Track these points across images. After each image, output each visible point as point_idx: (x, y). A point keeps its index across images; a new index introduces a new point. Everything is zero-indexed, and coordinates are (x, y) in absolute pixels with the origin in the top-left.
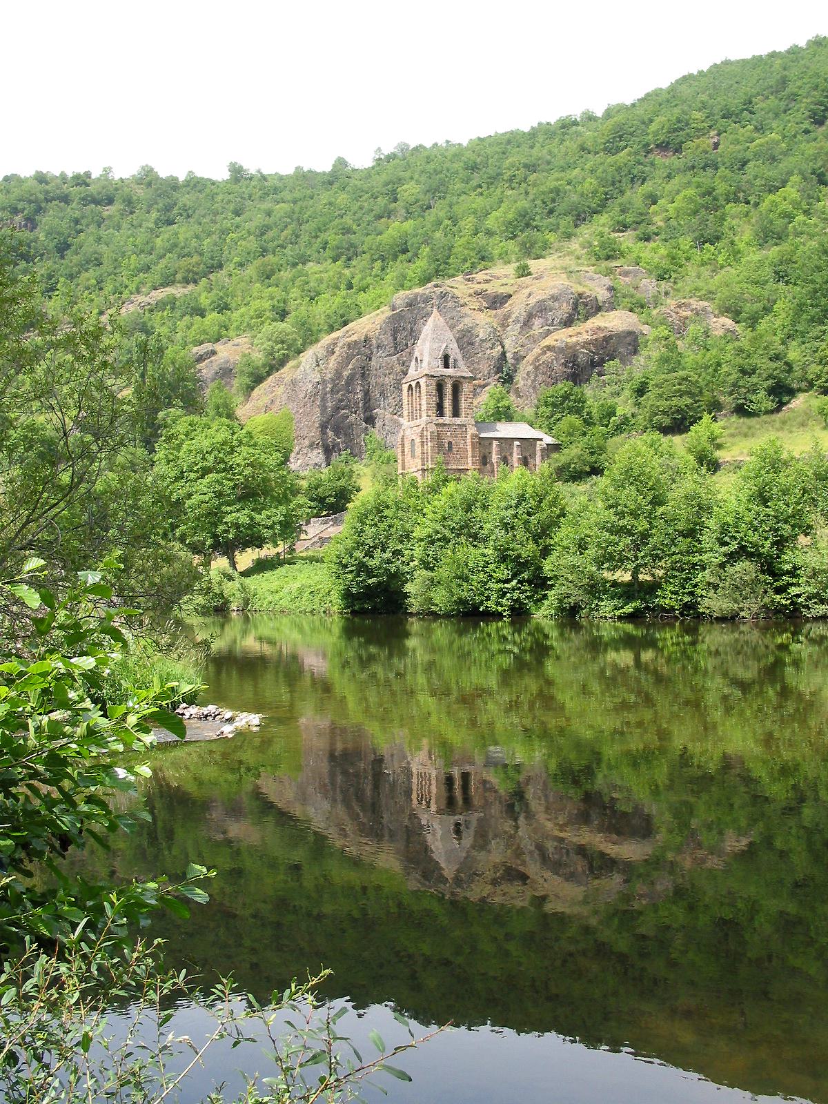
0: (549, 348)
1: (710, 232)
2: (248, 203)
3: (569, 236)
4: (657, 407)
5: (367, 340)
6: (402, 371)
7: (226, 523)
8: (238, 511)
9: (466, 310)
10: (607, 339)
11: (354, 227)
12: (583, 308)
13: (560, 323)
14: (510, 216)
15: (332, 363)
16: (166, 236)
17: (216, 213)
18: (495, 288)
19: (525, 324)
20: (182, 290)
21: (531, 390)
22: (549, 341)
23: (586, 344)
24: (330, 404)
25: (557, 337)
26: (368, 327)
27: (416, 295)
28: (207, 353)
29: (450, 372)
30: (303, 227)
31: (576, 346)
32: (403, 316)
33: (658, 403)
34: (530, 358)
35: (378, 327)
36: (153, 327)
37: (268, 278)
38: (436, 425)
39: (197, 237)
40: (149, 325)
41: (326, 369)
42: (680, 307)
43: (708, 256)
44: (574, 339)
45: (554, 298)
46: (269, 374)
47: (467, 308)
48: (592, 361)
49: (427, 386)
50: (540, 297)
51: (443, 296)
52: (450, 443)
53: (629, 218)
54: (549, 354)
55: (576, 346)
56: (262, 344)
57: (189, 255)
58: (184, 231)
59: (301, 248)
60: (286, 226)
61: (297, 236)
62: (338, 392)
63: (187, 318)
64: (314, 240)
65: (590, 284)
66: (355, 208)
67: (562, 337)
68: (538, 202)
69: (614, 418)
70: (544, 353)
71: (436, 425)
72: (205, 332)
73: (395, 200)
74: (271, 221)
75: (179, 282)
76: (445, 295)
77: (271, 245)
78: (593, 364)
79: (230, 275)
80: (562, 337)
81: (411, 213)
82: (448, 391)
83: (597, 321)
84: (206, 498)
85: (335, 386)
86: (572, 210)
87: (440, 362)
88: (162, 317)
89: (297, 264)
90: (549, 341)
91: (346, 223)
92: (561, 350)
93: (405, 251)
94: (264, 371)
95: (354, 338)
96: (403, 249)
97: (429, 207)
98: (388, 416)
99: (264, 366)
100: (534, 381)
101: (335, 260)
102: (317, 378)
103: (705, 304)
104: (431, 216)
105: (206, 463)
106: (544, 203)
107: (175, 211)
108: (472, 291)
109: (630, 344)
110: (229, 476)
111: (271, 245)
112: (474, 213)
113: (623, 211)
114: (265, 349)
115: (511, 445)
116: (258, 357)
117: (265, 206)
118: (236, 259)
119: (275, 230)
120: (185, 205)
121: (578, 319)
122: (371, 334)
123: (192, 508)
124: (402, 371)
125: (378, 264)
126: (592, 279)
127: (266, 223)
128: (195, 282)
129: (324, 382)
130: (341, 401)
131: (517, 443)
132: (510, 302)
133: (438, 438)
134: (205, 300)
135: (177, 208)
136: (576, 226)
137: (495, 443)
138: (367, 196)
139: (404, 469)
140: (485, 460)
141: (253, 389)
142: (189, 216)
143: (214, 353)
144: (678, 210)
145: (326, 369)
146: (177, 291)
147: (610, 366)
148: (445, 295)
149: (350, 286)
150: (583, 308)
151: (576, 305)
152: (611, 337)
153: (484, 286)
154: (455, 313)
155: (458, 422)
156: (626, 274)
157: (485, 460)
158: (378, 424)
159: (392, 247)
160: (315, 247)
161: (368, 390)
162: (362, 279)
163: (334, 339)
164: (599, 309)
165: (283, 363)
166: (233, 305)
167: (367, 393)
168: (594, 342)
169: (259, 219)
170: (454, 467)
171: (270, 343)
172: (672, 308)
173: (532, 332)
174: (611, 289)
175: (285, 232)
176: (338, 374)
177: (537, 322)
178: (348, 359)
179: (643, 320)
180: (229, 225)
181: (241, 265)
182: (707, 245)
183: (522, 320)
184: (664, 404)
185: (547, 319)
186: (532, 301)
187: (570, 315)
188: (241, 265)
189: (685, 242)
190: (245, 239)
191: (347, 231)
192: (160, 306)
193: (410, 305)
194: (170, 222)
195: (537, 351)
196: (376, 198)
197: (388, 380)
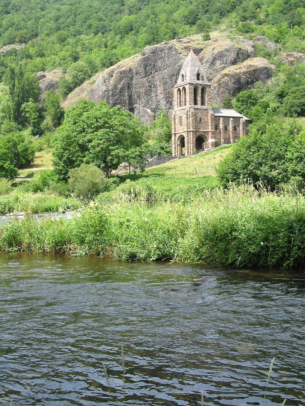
0: (226, 75)
1: (296, 20)
2: (47, 4)
3: (218, 23)
4: (294, 103)
5: (130, 70)
6: (149, 86)
7: (112, 155)
8: (117, 149)
9: (181, 56)
10: (255, 71)
11: (104, 18)
12: (241, 56)
13: (230, 63)
14: (186, 13)
15: (112, 81)
16: (8, 19)
17: (32, 9)
18: (194, 45)
19: (211, 63)
20: (19, 46)
21: (216, 96)
22: (225, 71)
23: (244, 73)
24: (111, 102)
25: (230, 70)
26: (131, 63)
27: (157, 48)
28: (41, 76)
29: (200, 82)
30: (77, 17)
31: (239, 74)
32: (150, 58)
33: (294, 101)
34: (215, 79)
35: (136, 63)
36: (7, 64)
37: (63, 41)
38: (194, 109)
39: (24, 20)
40: (5, 62)
41: (109, 84)
42: (288, 56)
43: (297, 31)
44: (238, 71)
45: (227, 50)
46: (75, 87)
47: (182, 55)
48: (248, 81)
49: (190, 89)
50: (220, 50)
51: (170, 48)
52: (200, 118)
53: (247, 15)
54: (226, 78)
55: (239, 74)
56: (71, 72)
57: (20, 29)
58: (16, 17)
59: (77, 28)
60: (69, 17)
61: (75, 22)
62: (115, 96)
63: (24, 60)
64: (84, 24)
65: (244, 44)
66: (103, 9)
67: (232, 70)
68: (200, 6)
69: (268, 109)
70: (223, 77)
71: (194, 109)
72: (36, 67)
73: (123, 5)
74: (60, 13)
75: (17, 42)
76: (171, 48)
77: (62, 26)
78: (248, 83)
79: (43, 40)
80: (232, 70)
81: (131, 12)
82: (199, 92)
83: (248, 62)
84: (101, 142)
85: (114, 92)
86: (218, 10)
87: (195, 77)
88: (11, 59)
89: (76, 35)
90: (225, 71)
91: (100, 16)
92: (233, 76)
93: (131, 30)
94: (72, 86)
95: (124, 69)
96: (129, 29)
97: (140, 9)
98: (141, 108)
99: (72, 83)
100: (218, 91)
101: (96, 34)
102: (104, 88)
103: (301, 54)
104: (144, 12)
105: (98, 124)
106: (203, 7)
107: (10, 7)
108: (183, 47)
109: (266, 74)
110: (111, 131)
111: (62, 26)
112: (165, 12)
113: (245, 11)
114: (73, 75)
115: (229, 120)
116: (69, 78)
117: (57, 6)
118: (46, 32)
119: (63, 18)
120: (15, 5)
121: (239, 61)
122: (132, 67)
123: (94, 147)
124: (149, 86)
125: (119, 36)
126: (243, 42)
127: (58, 14)
128: (25, 42)
129: (108, 90)
130: (117, 100)
131: (231, 119)
132: (202, 52)
133: (195, 115)
134: (32, 51)
135: (10, 6)
136: (221, 18)
137: (221, 119)
138: (108, 3)
139: (175, 131)
140: (216, 127)
141: (67, 94)
142: (17, 10)
143: (44, 76)
144: (274, 10)
145: (109, 84)
146: (17, 47)
147: (257, 83)
148: (171, 48)
149: (106, 46)
150: (241, 56)
151: (238, 54)
152: (256, 70)
153: (189, 45)
154: (176, 57)
155: (204, 108)
156: (259, 40)
157: (216, 127)
158: (136, 112)
159: (125, 27)
160: (85, 27)
161: (131, 95)
162: (112, 43)
163: (112, 70)
164: (249, 56)
165: (82, 81)
166: (46, 54)
167: (130, 97)
168: (249, 72)
169: (54, 13)
170: (202, 130)
171: (75, 71)
172: (284, 56)
173: (215, 67)
174: (253, 47)
175: (69, 20)
176: (115, 87)
177: (218, 63)
178: (121, 79)
179: (270, 62)
180: (39, 15)
181: (48, 35)
182: (296, 26)
183: (210, 61)
184: (297, 102)
185: (223, 61)
186: (216, 52)
187: (235, 59)
188: (48, 35)
189: (285, 25)
190: (48, 22)
191: (100, 20)
192: (10, 53)
193: (153, 53)
194: (8, 13)
195: (219, 76)
196: (113, 4)
197: (142, 90)
